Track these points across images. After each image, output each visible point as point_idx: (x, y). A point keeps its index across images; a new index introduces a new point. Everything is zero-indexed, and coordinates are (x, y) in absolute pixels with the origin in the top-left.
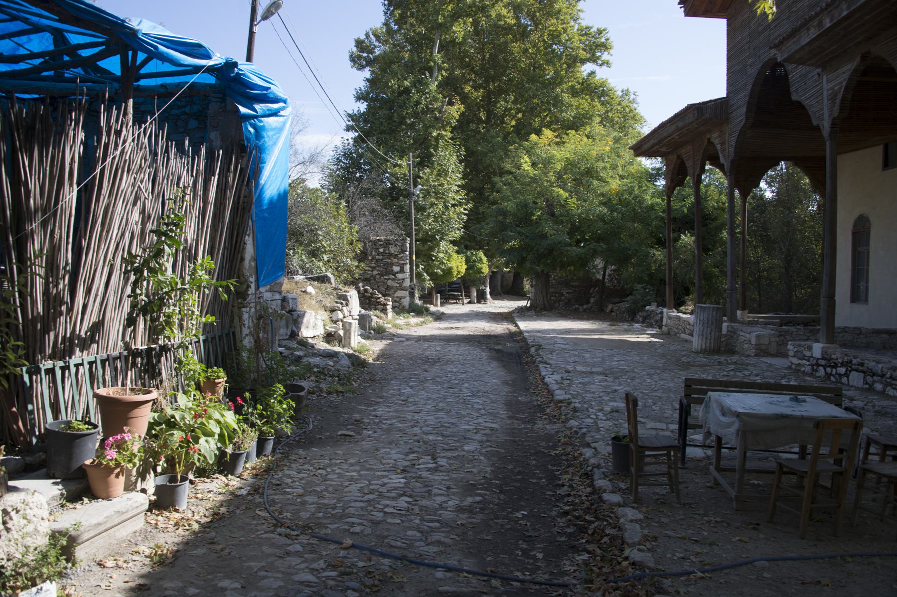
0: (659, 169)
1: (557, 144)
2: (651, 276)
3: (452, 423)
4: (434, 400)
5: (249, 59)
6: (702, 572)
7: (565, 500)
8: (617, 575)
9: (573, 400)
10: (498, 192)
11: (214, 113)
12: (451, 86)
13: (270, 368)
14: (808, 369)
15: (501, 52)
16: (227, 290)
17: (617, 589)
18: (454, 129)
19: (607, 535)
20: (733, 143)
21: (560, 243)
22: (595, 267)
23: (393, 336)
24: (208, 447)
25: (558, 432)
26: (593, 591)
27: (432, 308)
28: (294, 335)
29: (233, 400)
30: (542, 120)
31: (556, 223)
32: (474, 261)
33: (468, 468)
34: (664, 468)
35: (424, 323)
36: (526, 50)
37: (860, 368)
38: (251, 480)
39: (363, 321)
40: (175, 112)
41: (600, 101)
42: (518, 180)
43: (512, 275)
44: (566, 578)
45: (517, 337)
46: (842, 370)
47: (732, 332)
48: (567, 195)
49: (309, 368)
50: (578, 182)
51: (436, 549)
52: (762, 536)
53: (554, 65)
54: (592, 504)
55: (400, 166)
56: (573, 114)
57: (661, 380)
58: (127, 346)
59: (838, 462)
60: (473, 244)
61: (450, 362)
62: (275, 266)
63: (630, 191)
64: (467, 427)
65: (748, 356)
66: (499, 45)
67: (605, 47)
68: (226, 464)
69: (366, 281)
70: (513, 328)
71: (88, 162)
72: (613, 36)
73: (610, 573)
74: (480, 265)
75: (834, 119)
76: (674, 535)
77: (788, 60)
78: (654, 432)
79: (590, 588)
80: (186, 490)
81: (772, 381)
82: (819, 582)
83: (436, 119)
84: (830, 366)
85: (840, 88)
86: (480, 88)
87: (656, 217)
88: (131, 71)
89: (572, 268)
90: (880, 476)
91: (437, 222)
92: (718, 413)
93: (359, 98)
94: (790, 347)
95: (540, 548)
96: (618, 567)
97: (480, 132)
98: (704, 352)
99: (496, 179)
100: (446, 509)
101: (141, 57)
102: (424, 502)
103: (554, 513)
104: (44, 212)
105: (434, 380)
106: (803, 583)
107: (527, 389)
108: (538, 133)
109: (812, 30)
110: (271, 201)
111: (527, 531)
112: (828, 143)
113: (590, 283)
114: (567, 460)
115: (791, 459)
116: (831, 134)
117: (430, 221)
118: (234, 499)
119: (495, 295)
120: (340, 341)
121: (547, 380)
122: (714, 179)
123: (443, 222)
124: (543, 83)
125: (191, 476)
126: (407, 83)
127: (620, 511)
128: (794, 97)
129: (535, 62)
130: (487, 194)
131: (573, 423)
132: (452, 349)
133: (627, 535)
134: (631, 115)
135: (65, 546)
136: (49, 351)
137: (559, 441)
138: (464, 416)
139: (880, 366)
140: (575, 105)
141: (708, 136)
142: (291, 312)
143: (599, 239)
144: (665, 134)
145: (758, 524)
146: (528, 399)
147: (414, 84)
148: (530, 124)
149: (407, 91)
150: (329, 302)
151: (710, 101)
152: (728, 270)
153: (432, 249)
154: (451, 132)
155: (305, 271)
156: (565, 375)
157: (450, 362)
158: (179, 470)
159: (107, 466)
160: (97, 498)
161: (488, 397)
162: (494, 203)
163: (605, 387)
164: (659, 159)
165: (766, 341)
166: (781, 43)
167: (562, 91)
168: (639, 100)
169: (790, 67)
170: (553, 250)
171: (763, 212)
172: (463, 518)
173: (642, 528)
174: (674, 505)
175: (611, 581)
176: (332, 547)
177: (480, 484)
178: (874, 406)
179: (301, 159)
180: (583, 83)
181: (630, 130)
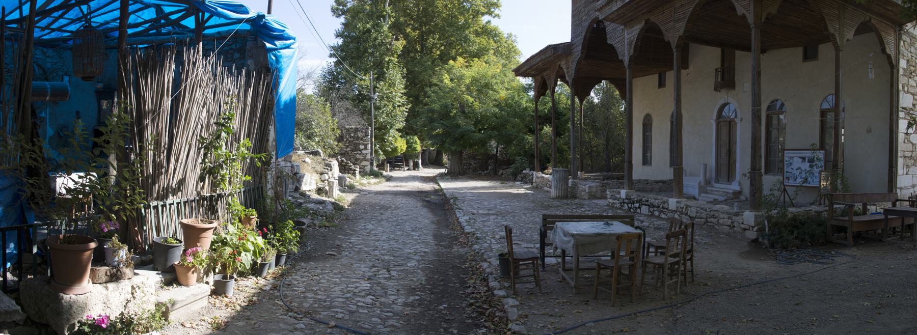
1: (467, 67)
2: (525, 152)
5: (269, 12)
11: (251, 49)
12: (397, 28)
13: (283, 209)
14: (618, 205)
15: (430, 6)
16: (260, 159)
18: (399, 56)
23: (360, 191)
24: (246, 259)
27: (385, 173)
28: (297, 189)
29: (261, 230)
34: (531, 272)
35: (379, 182)
36: (446, 6)
38: (272, 281)
39: (341, 180)
40: (226, 48)
45: (439, 192)
46: (637, 205)
47: (575, 185)
49: (307, 210)
50: (480, 91)
53: (464, 15)
55: (364, 80)
58: (199, 194)
59: (632, 259)
61: (397, 208)
62: (286, 146)
63: (513, 98)
68: (256, 270)
69: (343, 154)
70: (436, 187)
71: (177, 82)
77: (606, 19)
80: (232, 285)
83: (388, 49)
88: (200, 24)
90: (655, 264)
92: (562, 235)
93: (337, 36)
98: (558, 198)
99: (427, 89)
100: (396, 304)
101: (207, 15)
102: (382, 300)
104: (153, 114)
107: (448, 226)
108: (454, 59)
110: (286, 103)
113: (489, 157)
118: (261, 292)
119: (425, 165)
120: (326, 194)
122: (562, 90)
124: (457, 27)
125: (235, 276)
126: (368, 26)
127: (505, 301)
131: (476, 247)
133: (509, 315)
135: (164, 312)
136: (155, 195)
140: (478, 42)
142: (296, 174)
143: (493, 128)
147: (373, 27)
149: (369, 31)
150: (320, 168)
153: (385, 134)
155: (304, 148)
156: (472, 216)
157: (397, 208)
158: (229, 271)
159: (187, 266)
160: (181, 285)
162: (426, 104)
165: (595, 190)
166: (601, 8)
168: (518, 40)
169: (606, 23)
172: (408, 311)
173: (518, 310)
176: (323, 326)
179: (301, 76)
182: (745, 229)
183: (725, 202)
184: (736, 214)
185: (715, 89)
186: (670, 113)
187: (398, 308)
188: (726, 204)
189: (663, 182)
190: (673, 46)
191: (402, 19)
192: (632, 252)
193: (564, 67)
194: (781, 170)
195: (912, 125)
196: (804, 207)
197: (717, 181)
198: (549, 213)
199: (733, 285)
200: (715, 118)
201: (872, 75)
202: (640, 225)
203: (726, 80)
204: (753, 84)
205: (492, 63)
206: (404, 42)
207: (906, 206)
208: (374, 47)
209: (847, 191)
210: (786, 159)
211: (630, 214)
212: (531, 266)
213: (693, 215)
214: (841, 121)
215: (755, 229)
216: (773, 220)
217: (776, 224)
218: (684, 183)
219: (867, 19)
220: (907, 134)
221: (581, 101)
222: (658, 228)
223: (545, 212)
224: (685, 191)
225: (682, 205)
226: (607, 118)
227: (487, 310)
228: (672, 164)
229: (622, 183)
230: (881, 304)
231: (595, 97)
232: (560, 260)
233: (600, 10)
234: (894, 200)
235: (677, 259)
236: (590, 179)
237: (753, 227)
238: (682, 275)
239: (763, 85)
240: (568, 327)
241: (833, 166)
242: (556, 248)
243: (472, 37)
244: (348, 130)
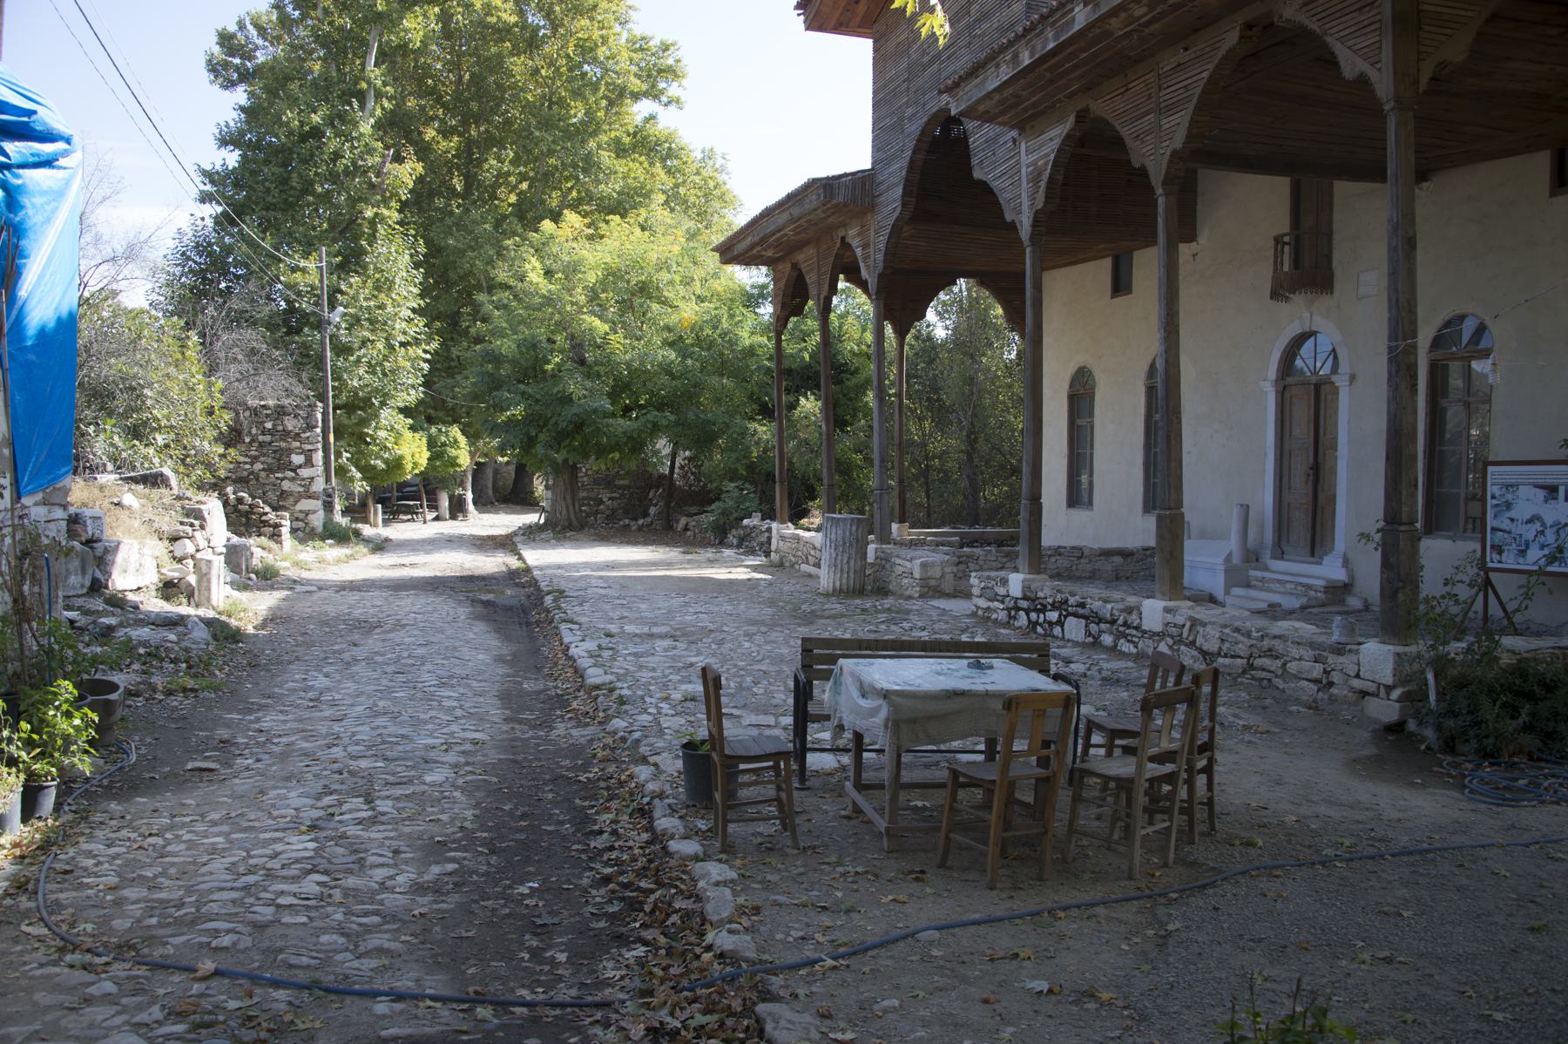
0: (764, 287)
1: (590, 238)
2: (751, 467)
12: (398, 128)
14: (1002, 616)
15: (491, 71)
20: (882, 246)
27: (367, 530)
28: (97, 587)
34: (770, 791)
36: (536, 71)
37: (1081, 611)
39: (234, 557)
45: (520, 578)
46: (1053, 616)
47: (884, 560)
49: (129, 647)
50: (626, 306)
53: (585, 99)
55: (304, 270)
57: (767, 643)
59: (1043, 762)
61: (398, 626)
63: (715, 323)
65: (910, 598)
69: (241, 481)
70: (514, 563)
75: (1037, 212)
77: (968, 113)
83: (372, 186)
85: (1046, 164)
92: (855, 693)
93: (224, 142)
98: (839, 593)
99: (481, 297)
107: (538, 669)
108: (556, 217)
109: (1003, 68)
110: (42, 332)
112: (1028, 250)
113: (649, 481)
119: (482, 503)
120: (190, 596)
122: (853, 306)
124: (565, 131)
127: (698, 868)
128: (977, 174)
131: (618, 723)
133: (709, 908)
139: (1109, 606)
140: (619, 173)
141: (841, 233)
142: (89, 542)
149: (316, 133)
150: (169, 523)
151: (846, 175)
153: (364, 422)
156: (605, 641)
157: (398, 626)
162: (479, 340)
164: (764, 269)
166: (956, 85)
168: (730, 167)
169: (970, 125)
173: (735, 894)
176: (176, 978)
178: (1100, 671)
179: (107, 252)
182: (1364, 694)
183: (1302, 612)
184: (1339, 650)
185: (1276, 294)
188: (1305, 620)
189: (1125, 554)
191: (411, 103)
192: (1046, 744)
193: (855, 243)
194: (1477, 525)
197: (1280, 554)
198: (815, 634)
199: (1329, 852)
200: (1272, 373)
202: (1063, 670)
203: (1306, 267)
204: (1393, 274)
205: (660, 229)
206: (420, 168)
208: (333, 177)
211: (1032, 640)
213: (1212, 646)
215: (1396, 694)
216: (1453, 672)
217: (1461, 684)
218: (1187, 558)
221: (901, 333)
222: (1110, 681)
223: (805, 631)
224: (1186, 581)
225: (1180, 620)
226: (971, 381)
227: (648, 899)
229: (1012, 556)
231: (937, 324)
232: (846, 759)
235: (1169, 768)
236: (922, 543)
237: (1389, 689)
238: (1183, 811)
240: (870, 940)
243: (606, 158)
244: (255, 412)
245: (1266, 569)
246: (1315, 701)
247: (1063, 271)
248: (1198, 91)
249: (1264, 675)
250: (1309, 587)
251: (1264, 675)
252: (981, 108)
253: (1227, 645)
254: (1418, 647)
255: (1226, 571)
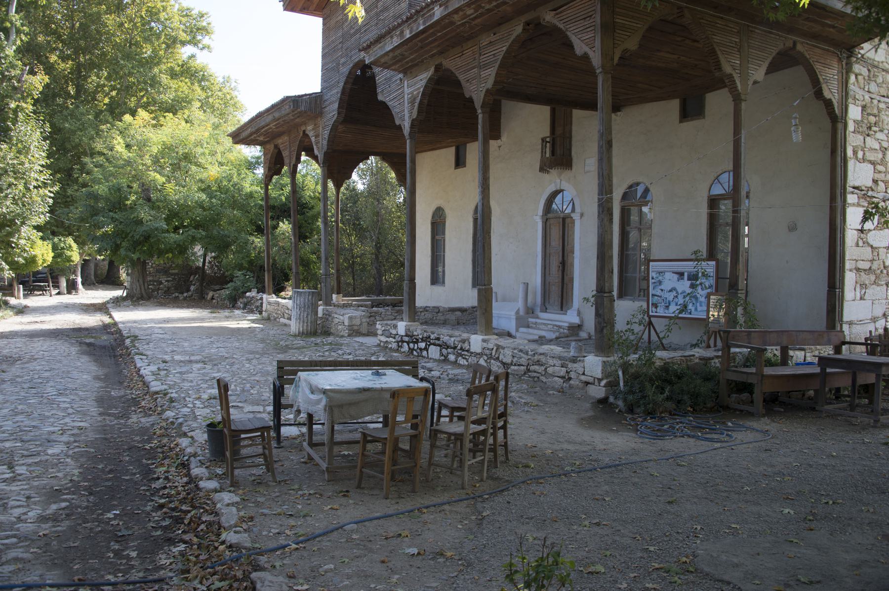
0: (258, 158)
1: (155, 126)
2: (251, 262)
3: (34, 427)
4: (12, 403)
6: (297, 544)
7: (161, 494)
8: (213, 560)
9: (170, 391)
10: (88, 173)
12: (32, 53)
14: (394, 346)
15: (93, 22)
17: (214, 574)
18: (36, 102)
19: (203, 523)
20: (326, 136)
21: (157, 229)
22: (194, 254)
25: (153, 425)
26: (190, 581)
27: (13, 301)
30: (139, 100)
31: (153, 208)
32: (63, 248)
33: (52, 473)
34: (259, 449)
36: (121, 25)
37: (437, 342)
41: (200, 86)
42: (110, 162)
43: (106, 263)
44: (162, 572)
45: (110, 329)
46: (422, 345)
47: (328, 315)
48: (164, 179)
50: (176, 167)
51: (12, 568)
52: (351, 501)
53: (152, 43)
54: (188, 494)
56: (172, 97)
57: (259, 364)
59: (414, 427)
60: (61, 230)
61: (33, 359)
64: (52, 429)
65: (342, 336)
66: (90, 15)
67: (205, 30)
70: (107, 320)
72: (215, 20)
73: (206, 560)
74: (68, 253)
75: (413, 120)
76: (270, 512)
77: (375, 63)
78: (251, 416)
79: (187, 578)
81: (363, 358)
82: (400, 535)
84: (413, 342)
85: (418, 93)
86: (68, 59)
87: (255, 205)
89: (170, 255)
90: (450, 434)
91: (17, 205)
92: (308, 392)
94: (378, 326)
95: (134, 546)
96: (215, 552)
97: (67, 108)
98: (302, 334)
99: (87, 160)
103: (149, 508)
105: (13, 381)
106: (386, 539)
107: (121, 383)
108: (133, 113)
109: (395, 39)
111: (120, 531)
113: (190, 271)
114: (163, 452)
115: (377, 428)
116: (411, 133)
117: (8, 203)
121: (142, 372)
122: (309, 170)
123: (24, 205)
124: (140, 61)
127: (217, 496)
128: (380, 98)
129: (132, 39)
130: (75, 176)
131: (169, 414)
132: (35, 345)
133: (223, 519)
134: (232, 102)
137: (155, 434)
138: (48, 417)
139: (452, 339)
141: (303, 128)
143: (198, 226)
144: (263, 124)
145: (347, 491)
146: (122, 393)
148: (125, 103)
151: (306, 95)
152: (323, 256)
153: (11, 234)
154: (33, 105)
156: (162, 366)
157: (33, 359)
161: (76, 394)
162: (85, 185)
163: (203, 374)
164: (259, 148)
166: (369, 47)
167: (160, 72)
169: (377, 70)
170: (149, 237)
171: (355, 203)
172: (46, 528)
173: (239, 510)
174: (271, 483)
175: (208, 567)
177: (66, 489)
178: (448, 375)
180: (182, 66)
181: (230, 117)
182: (587, 383)
183: (557, 341)
184: (574, 360)
185: (542, 170)
186: (473, 207)
187: (25, 528)
188: (558, 345)
189: (462, 310)
190: (478, 104)
191: (41, 38)
192: (415, 417)
193: (311, 134)
194: (645, 293)
195: (872, 214)
196: (681, 350)
197: (544, 309)
198: (288, 359)
200: (540, 212)
201: (797, 137)
202: (427, 375)
203: (558, 154)
204: (600, 160)
206: (47, 79)
207: (860, 353)
209: (753, 326)
210: (652, 274)
211: (411, 358)
212: (259, 440)
213: (508, 360)
214: (743, 213)
215: (603, 383)
216: (632, 370)
217: (636, 376)
219: (789, 44)
220: (862, 231)
221: (338, 186)
222: (453, 380)
223: (281, 357)
225: (490, 346)
226: (378, 214)
227: (188, 517)
228: (475, 283)
229: (400, 312)
230: (814, 514)
231: (358, 181)
232: (304, 430)
233: (366, 49)
234: (838, 343)
235: (483, 427)
236: (350, 305)
237: (600, 380)
238: (490, 450)
239: (615, 161)
240: (317, 532)
241: (730, 286)
242: (299, 412)
243: (165, 79)
245: (538, 318)
246: (562, 388)
247: (429, 153)
248: (501, 57)
249: (535, 374)
250: (560, 327)
251: (535, 374)
252: (383, 61)
253: (516, 359)
254: (614, 358)
255: (517, 319)
